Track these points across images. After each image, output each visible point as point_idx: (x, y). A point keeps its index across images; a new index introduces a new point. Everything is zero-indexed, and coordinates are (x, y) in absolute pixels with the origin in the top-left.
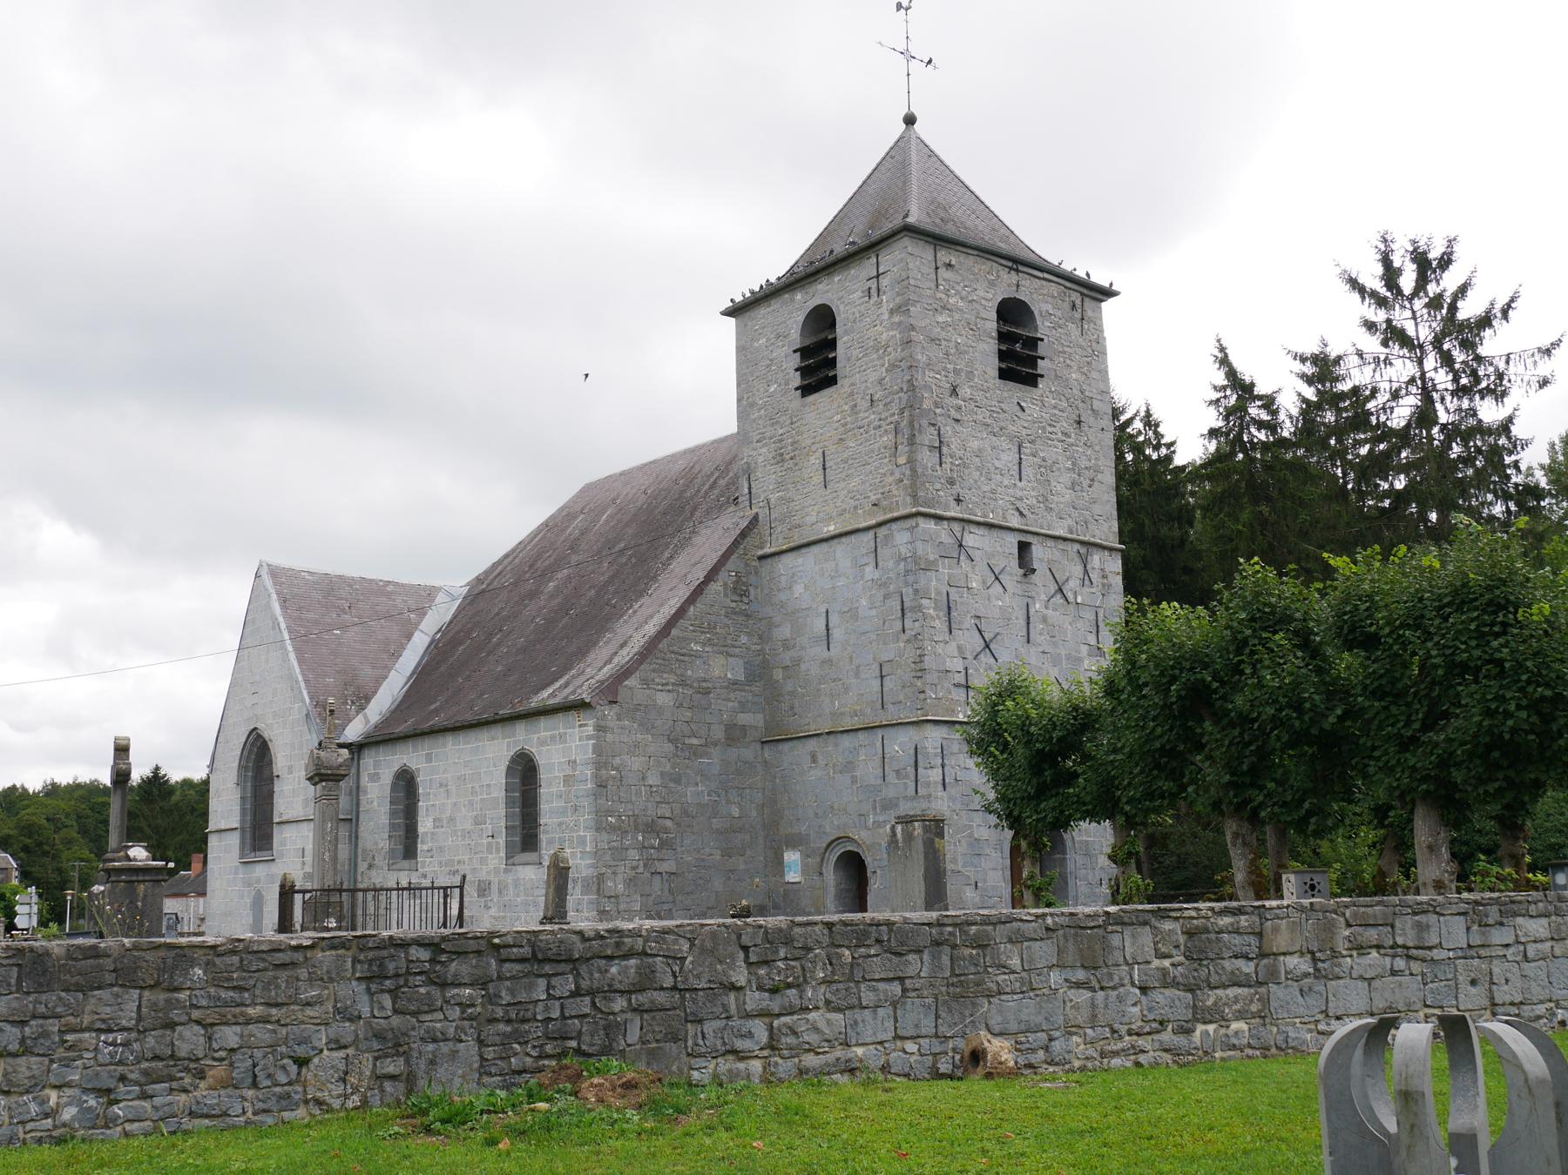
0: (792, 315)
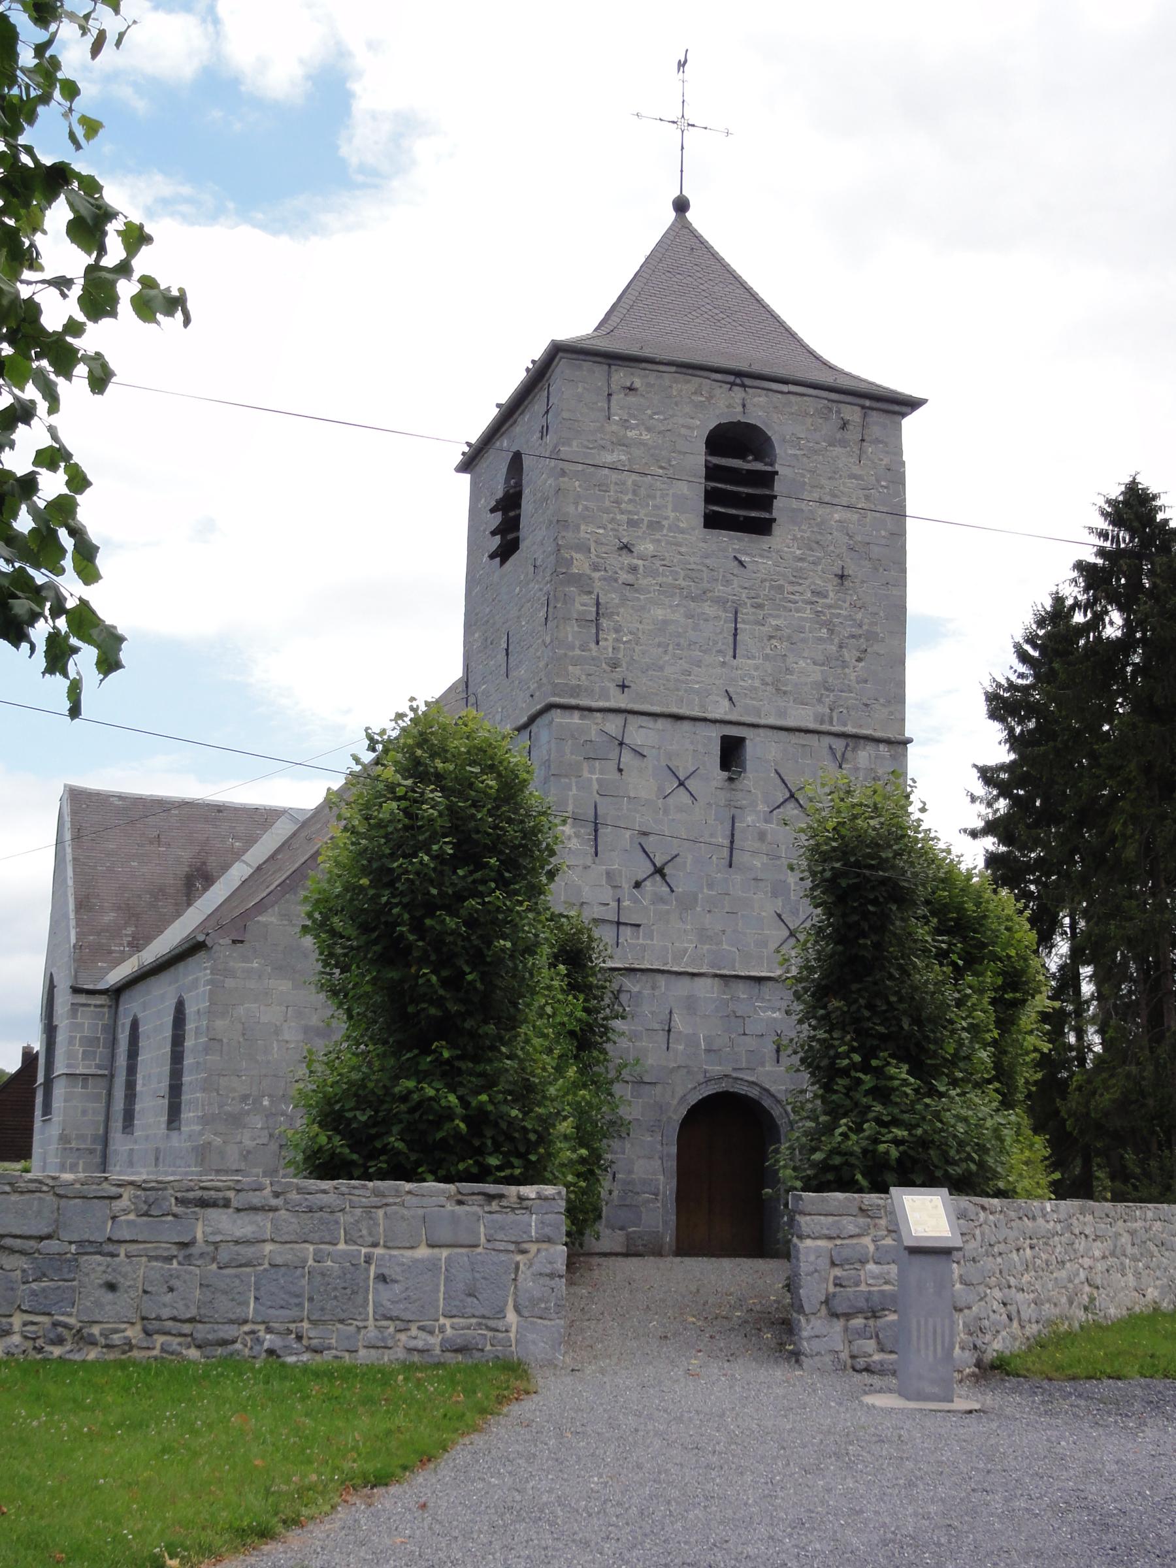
0: (497, 465)
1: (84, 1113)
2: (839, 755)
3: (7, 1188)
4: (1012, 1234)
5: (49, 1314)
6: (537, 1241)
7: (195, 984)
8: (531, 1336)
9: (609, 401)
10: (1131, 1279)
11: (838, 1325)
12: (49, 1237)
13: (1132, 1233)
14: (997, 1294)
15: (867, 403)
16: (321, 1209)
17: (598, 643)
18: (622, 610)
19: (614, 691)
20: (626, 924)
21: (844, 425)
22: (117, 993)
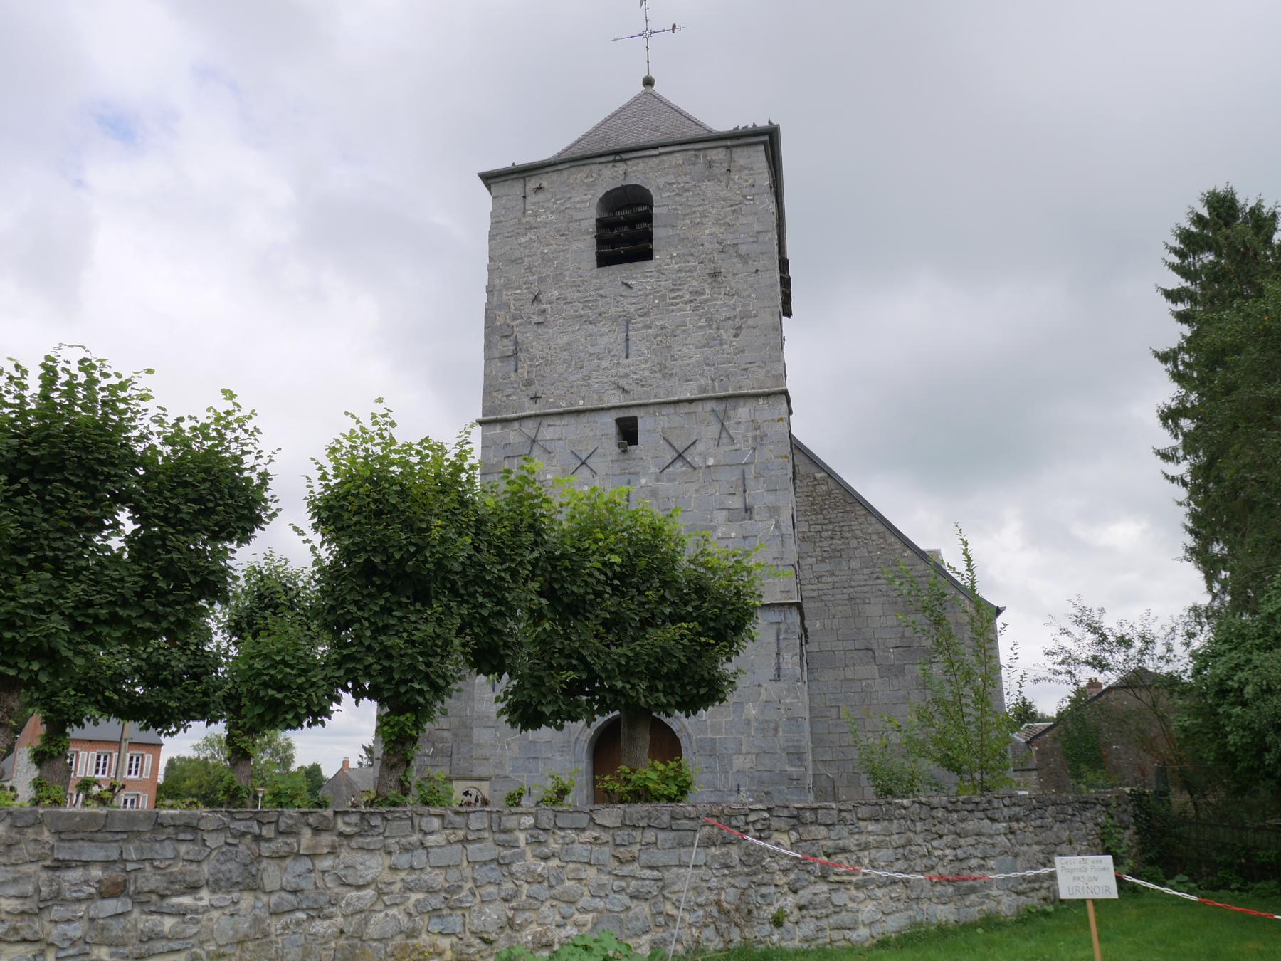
15: (729, 143)
19: (527, 402)
21: (710, 165)
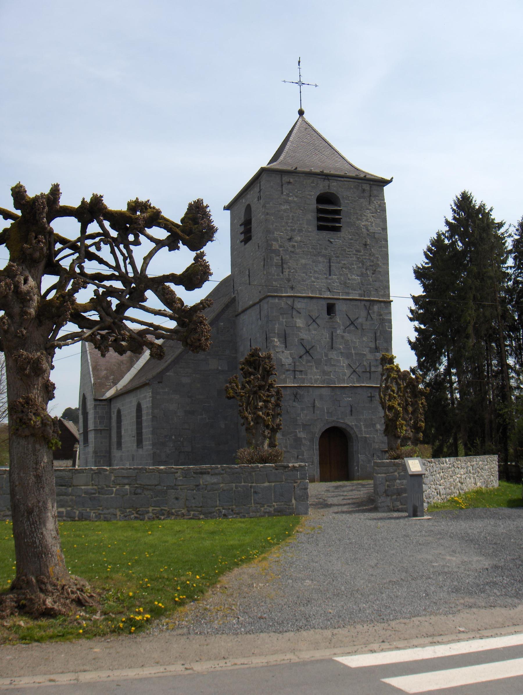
0: (241, 209)
1: (101, 443)
2: (368, 307)
3: (145, 472)
4: (437, 469)
5: (159, 507)
6: (300, 479)
7: (145, 397)
8: (300, 507)
9: (282, 187)
10: (473, 480)
11: (389, 499)
12: (158, 485)
13: (472, 466)
14: (434, 486)
15: (372, 183)
16: (236, 473)
17: (283, 273)
18: (290, 261)
20: (298, 371)
22: (110, 400)
